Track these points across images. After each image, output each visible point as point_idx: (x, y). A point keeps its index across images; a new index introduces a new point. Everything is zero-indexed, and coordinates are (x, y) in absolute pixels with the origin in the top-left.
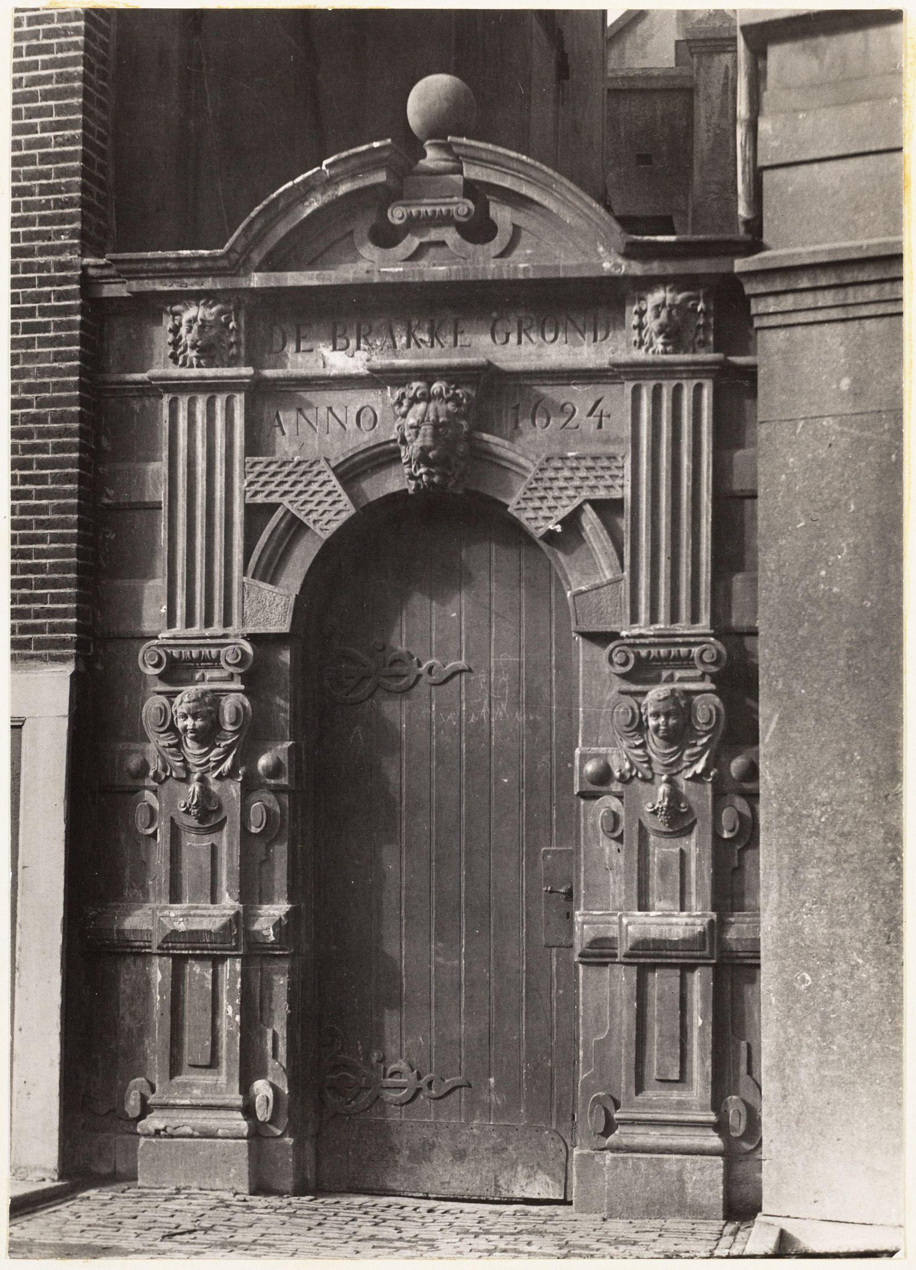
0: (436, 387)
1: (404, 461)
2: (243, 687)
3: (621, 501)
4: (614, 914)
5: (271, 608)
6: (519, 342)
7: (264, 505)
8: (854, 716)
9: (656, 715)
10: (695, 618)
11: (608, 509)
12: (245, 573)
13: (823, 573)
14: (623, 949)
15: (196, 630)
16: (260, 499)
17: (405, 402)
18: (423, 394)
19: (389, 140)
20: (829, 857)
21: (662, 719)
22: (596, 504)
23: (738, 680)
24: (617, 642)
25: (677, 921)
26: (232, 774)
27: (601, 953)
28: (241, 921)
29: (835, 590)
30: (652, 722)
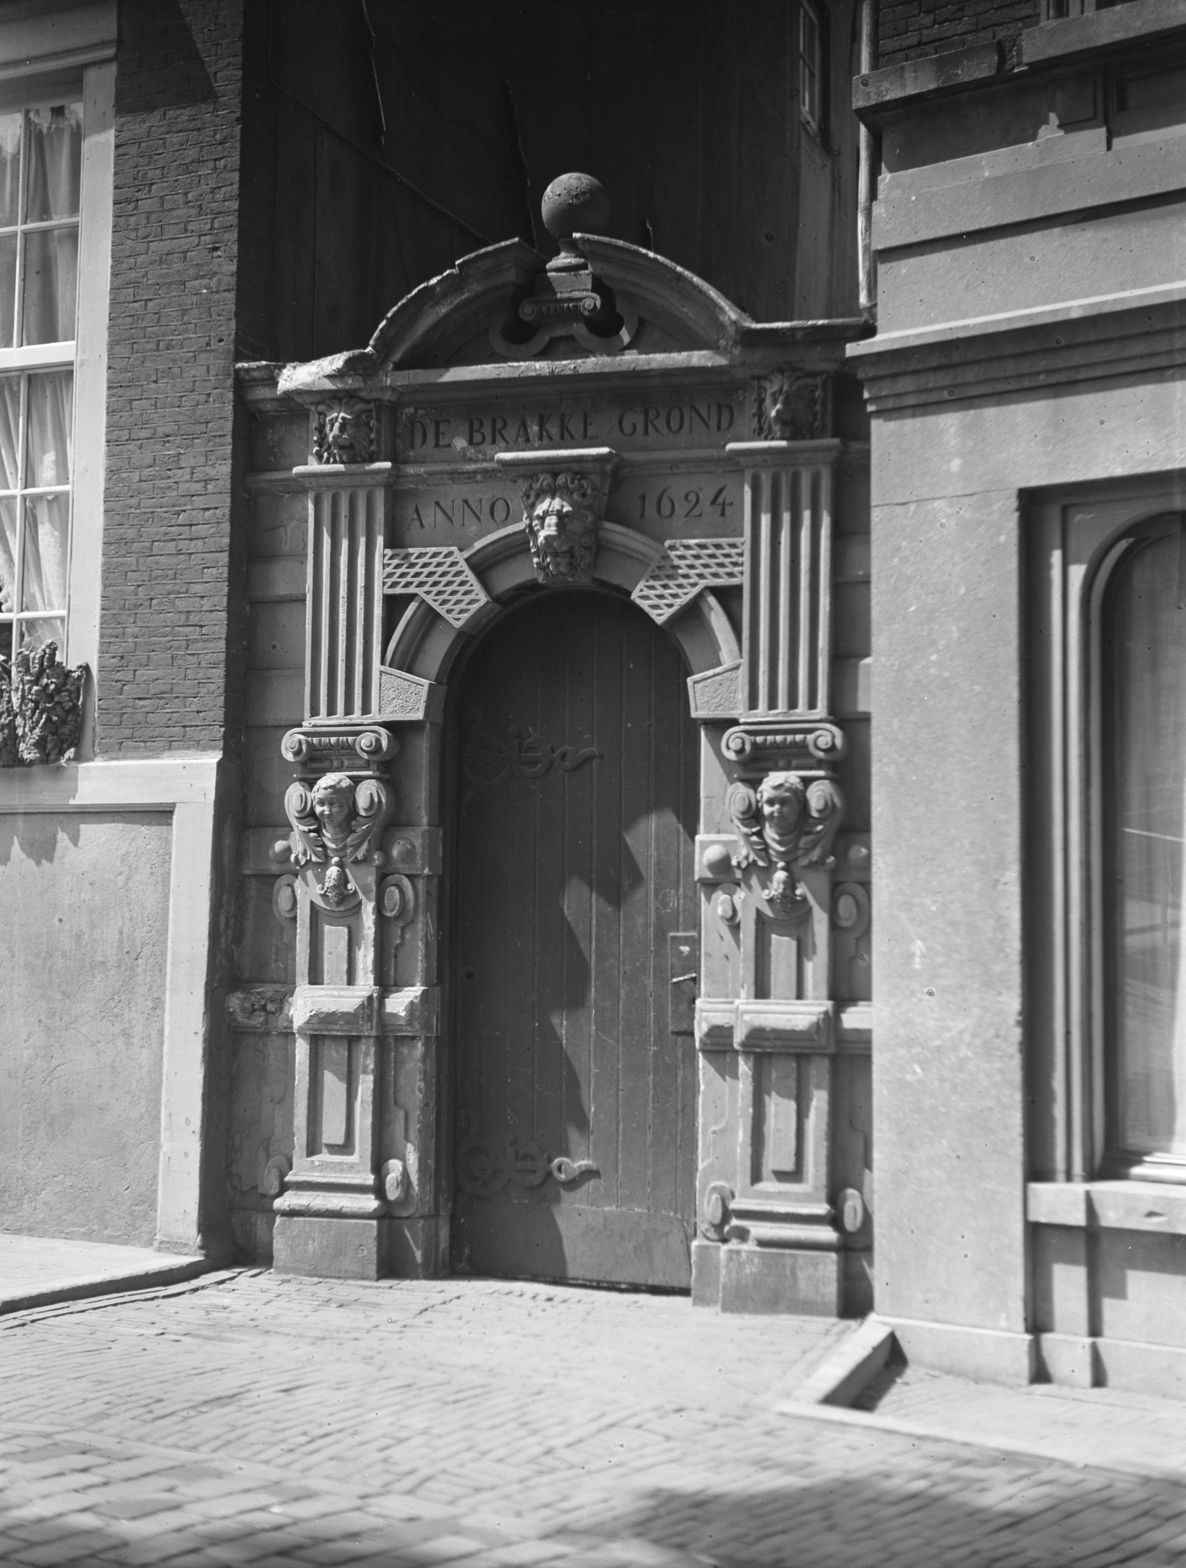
0: (561, 480)
1: (533, 550)
2: (378, 774)
3: (739, 588)
4: (727, 1005)
5: (403, 697)
6: (646, 432)
7: (401, 595)
8: (963, 803)
9: (771, 802)
10: (812, 705)
11: (728, 597)
12: (383, 663)
13: (934, 657)
14: (738, 1038)
15: (339, 718)
16: (398, 590)
17: (533, 494)
18: (549, 485)
19: (517, 239)
20: (939, 947)
21: (777, 807)
22: (716, 591)
23: (849, 769)
24: (736, 729)
25: (797, 1014)
26: (367, 860)
27: (719, 1044)
28: (373, 1007)
29: (946, 674)
30: (767, 810)
